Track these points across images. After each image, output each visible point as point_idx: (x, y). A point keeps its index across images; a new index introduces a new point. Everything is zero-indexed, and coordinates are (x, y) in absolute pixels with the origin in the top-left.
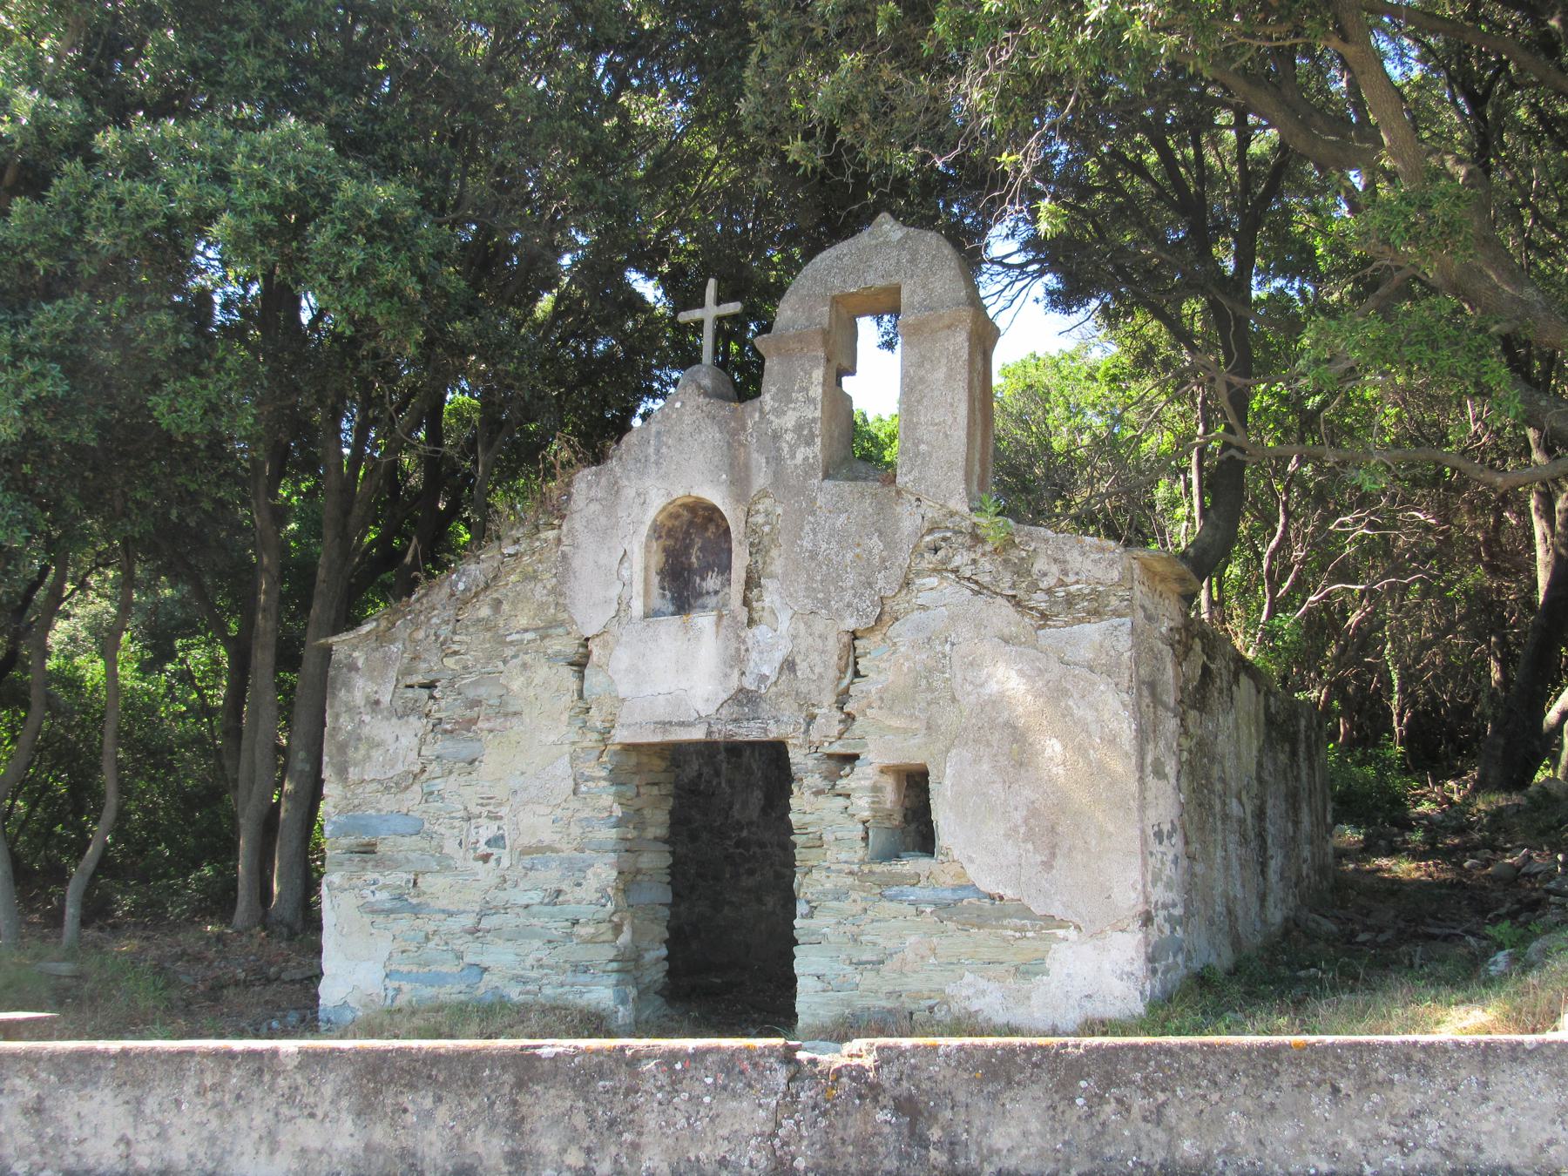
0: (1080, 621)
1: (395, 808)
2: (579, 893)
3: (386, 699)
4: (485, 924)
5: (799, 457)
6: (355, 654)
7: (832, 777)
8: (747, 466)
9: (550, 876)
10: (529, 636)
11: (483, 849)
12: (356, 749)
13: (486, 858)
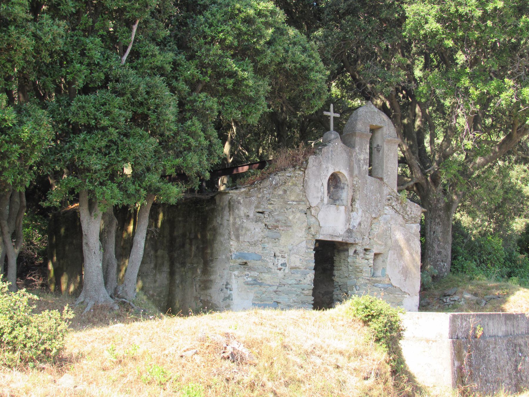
0: (412, 223)
1: (253, 251)
2: (305, 281)
3: (251, 215)
6: (239, 198)
8: (353, 167)
9: (298, 276)
10: (294, 203)
11: (280, 267)
12: (242, 230)
13: (280, 269)
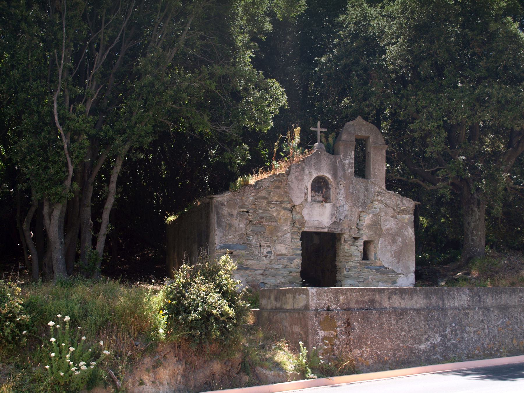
4: (266, 272)
5: (349, 171)
7: (354, 242)
10: (278, 202)
11: (265, 254)
13: (266, 257)
